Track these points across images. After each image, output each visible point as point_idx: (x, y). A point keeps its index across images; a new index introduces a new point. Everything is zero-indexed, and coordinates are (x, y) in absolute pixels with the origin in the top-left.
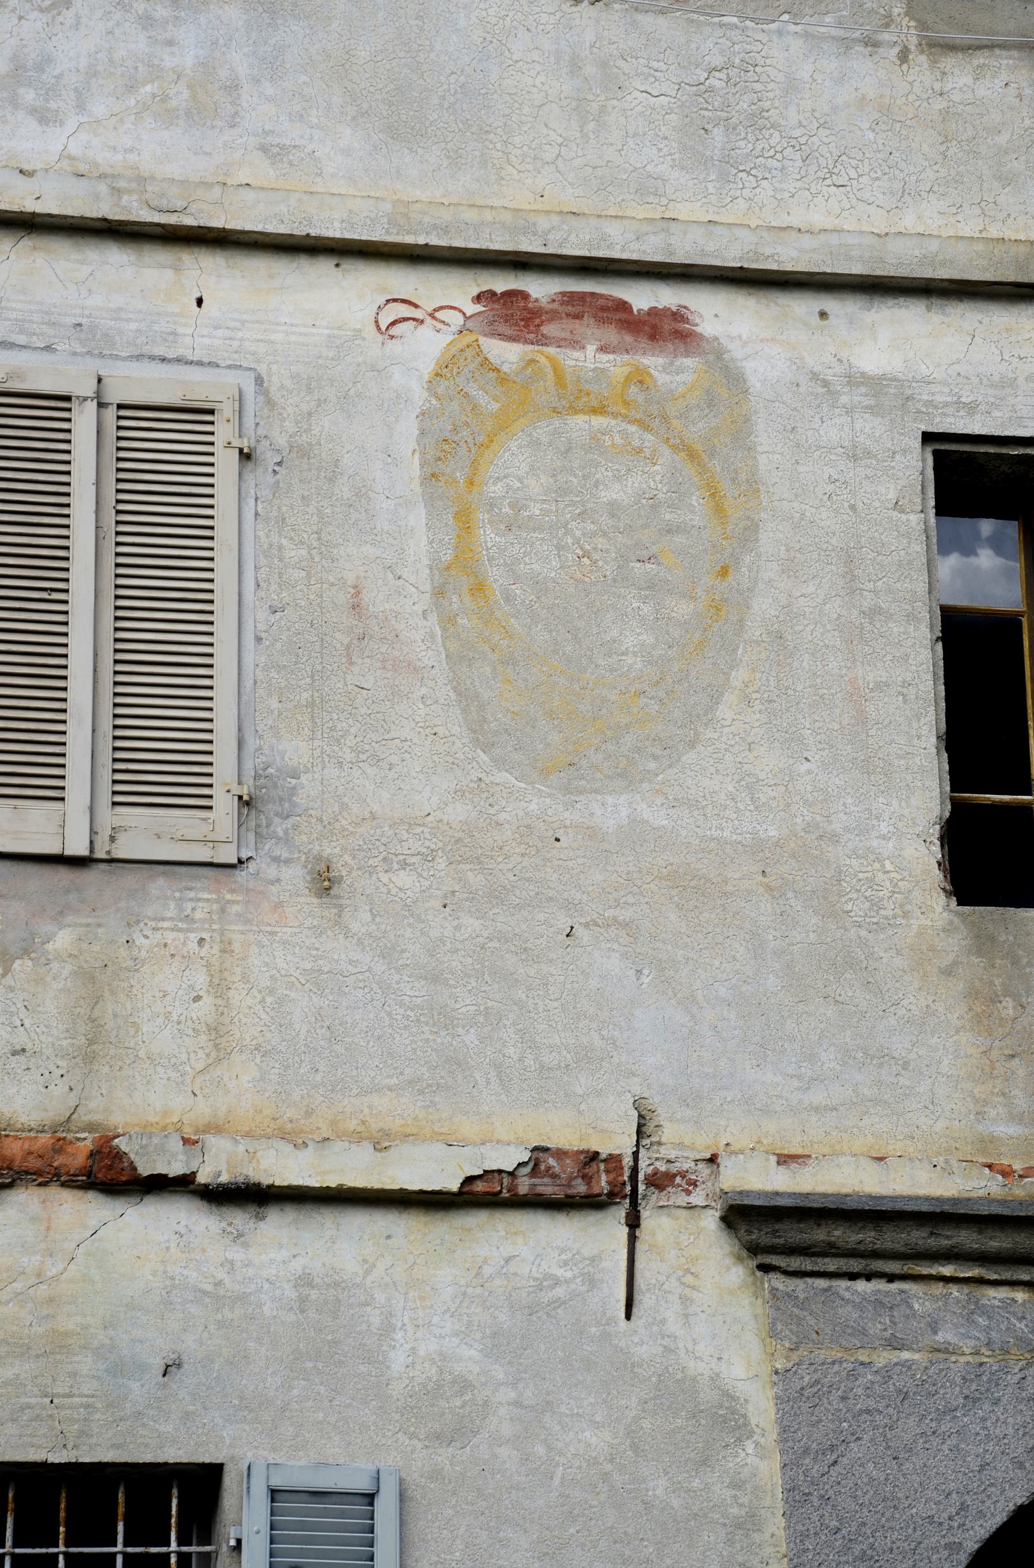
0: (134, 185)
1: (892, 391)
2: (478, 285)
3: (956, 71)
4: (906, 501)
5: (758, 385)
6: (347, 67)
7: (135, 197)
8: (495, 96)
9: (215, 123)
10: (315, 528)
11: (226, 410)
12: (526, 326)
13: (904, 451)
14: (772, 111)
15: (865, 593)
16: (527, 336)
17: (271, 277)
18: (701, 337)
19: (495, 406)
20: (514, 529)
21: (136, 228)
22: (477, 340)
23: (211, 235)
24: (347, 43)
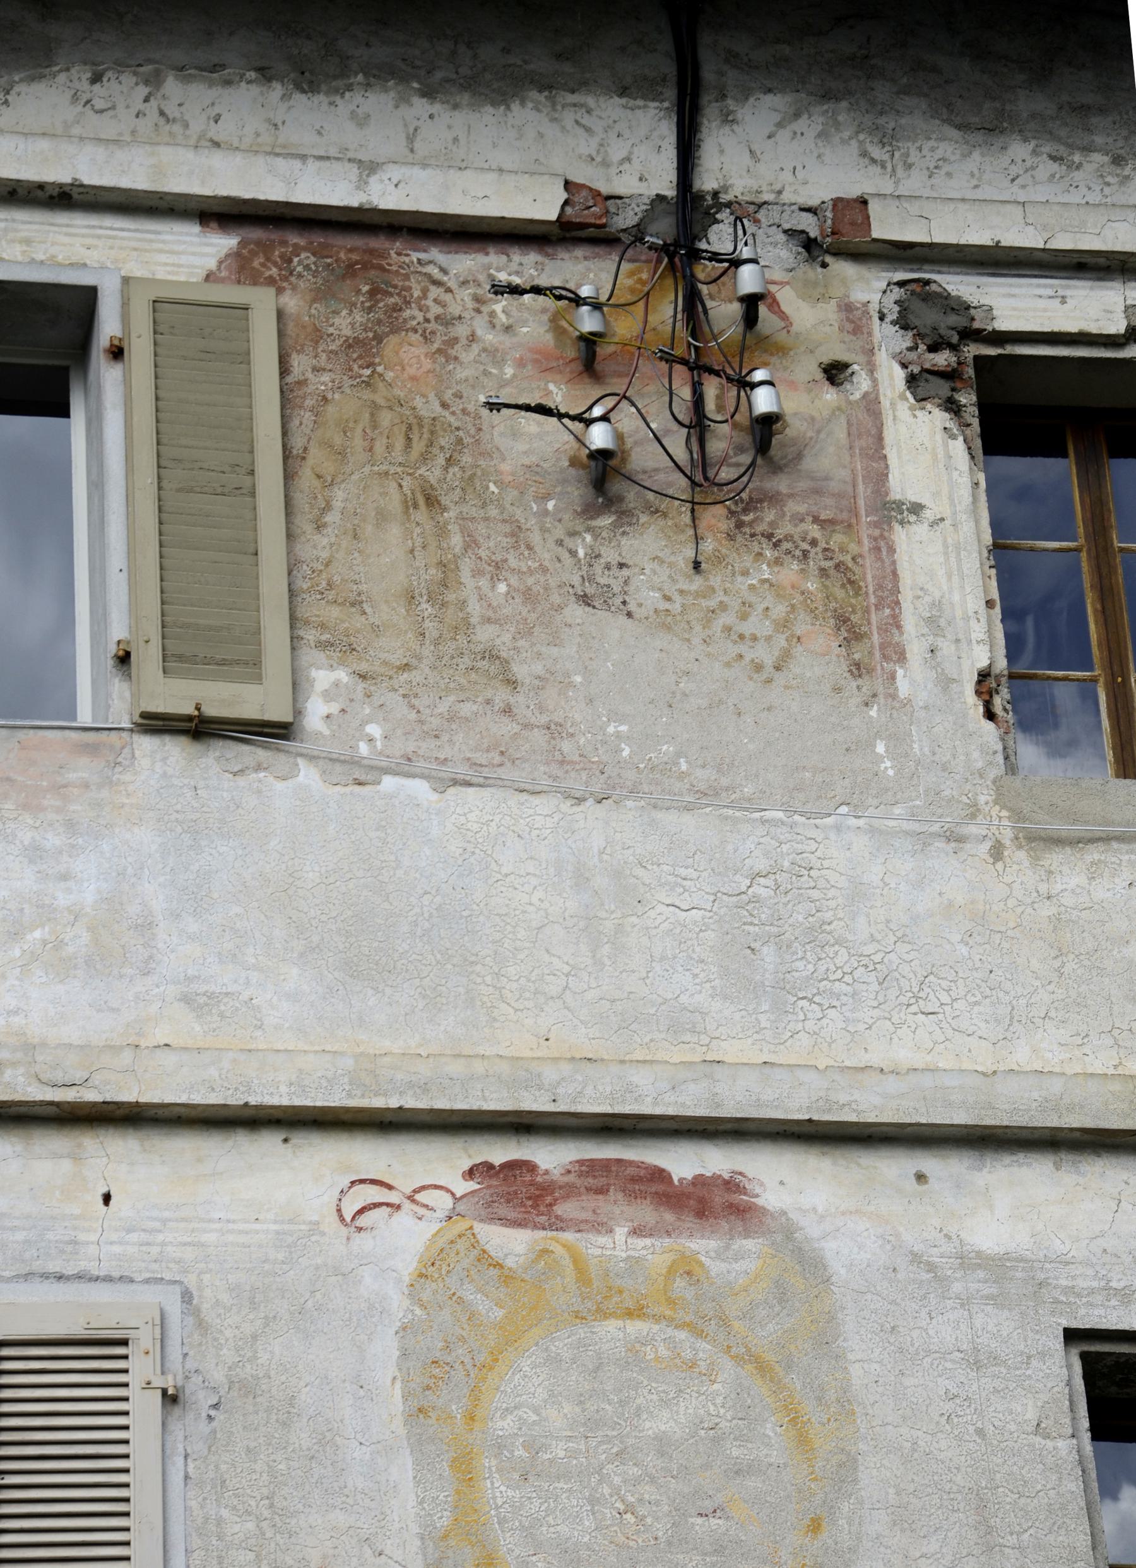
0: (19, 1055)
1: (1019, 1275)
2: (470, 1157)
3: (1065, 869)
4: (1051, 1422)
5: (843, 1271)
6: (290, 892)
7: (21, 1070)
8: (481, 918)
9: (123, 971)
10: (265, 1491)
11: (144, 1339)
12: (535, 1206)
13: (1043, 1355)
14: (835, 923)
15: (1007, 1551)
16: (537, 1219)
17: (199, 1160)
18: (764, 1211)
19: (499, 1313)
20: (531, 1478)
21: (23, 1110)
22: (471, 1228)
23: (120, 1112)
24: (290, 863)
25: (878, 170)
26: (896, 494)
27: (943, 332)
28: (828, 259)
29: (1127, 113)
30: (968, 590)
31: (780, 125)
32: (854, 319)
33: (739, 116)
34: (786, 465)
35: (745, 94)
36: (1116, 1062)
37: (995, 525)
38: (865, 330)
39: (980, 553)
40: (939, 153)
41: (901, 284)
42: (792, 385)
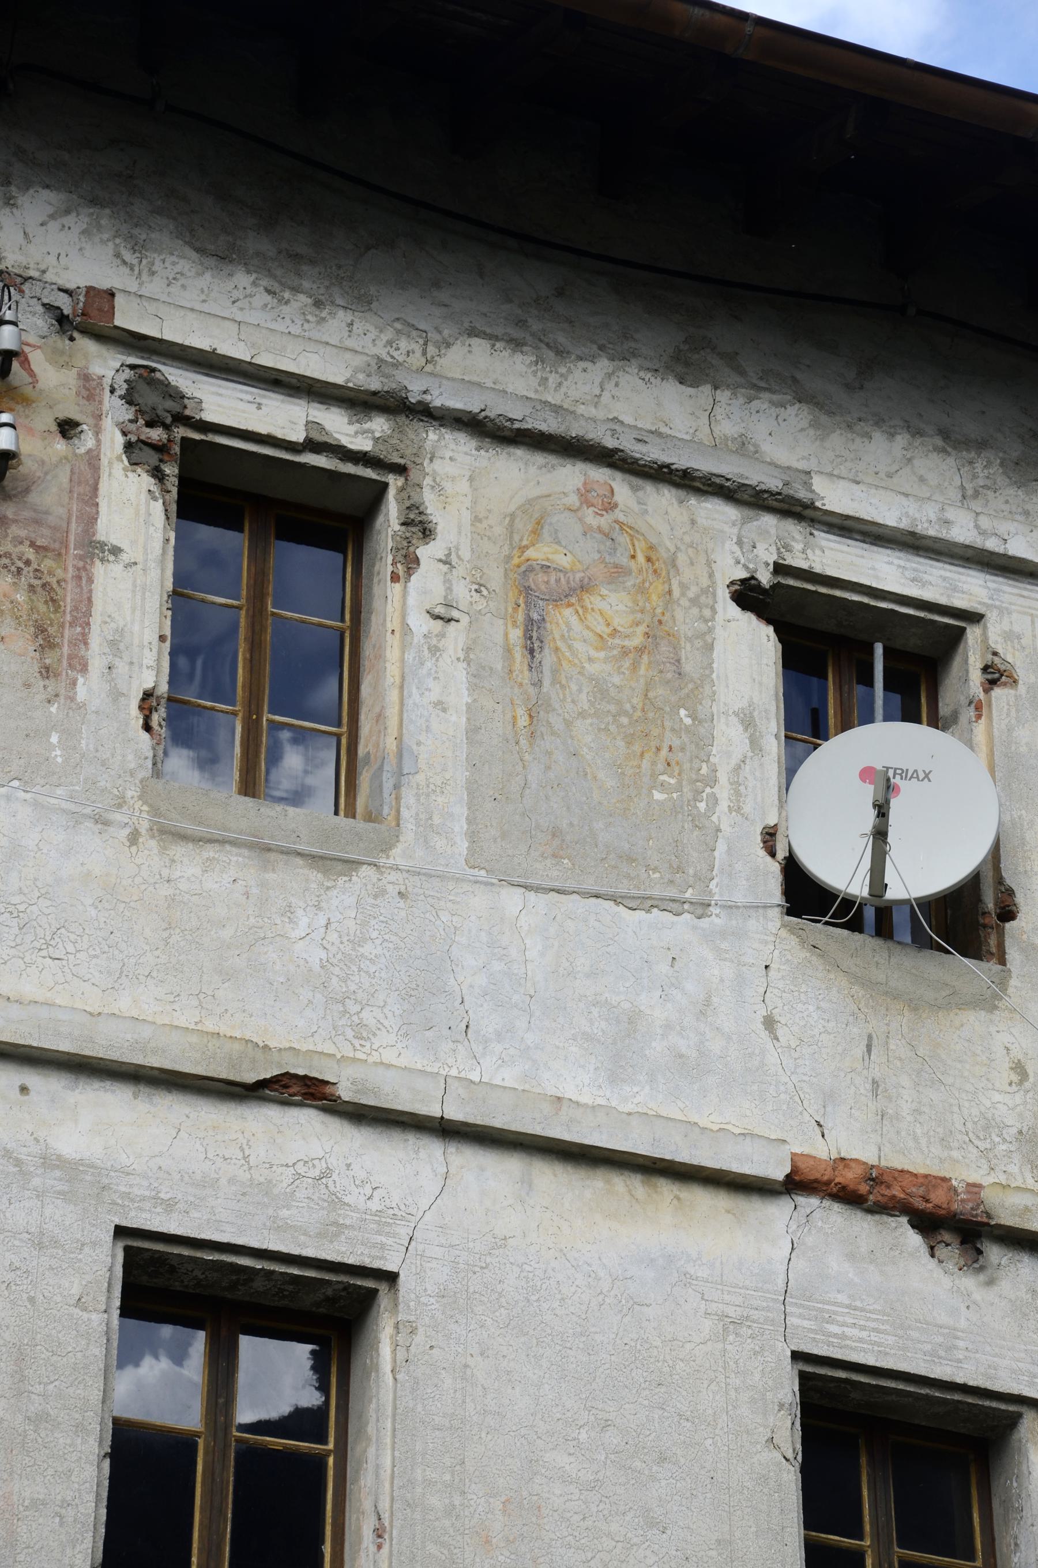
1: (88, 1178)
4: (90, 1298)
13: (94, 1244)
15: (33, 1396)
25: (127, 271)
26: (101, 535)
27: (160, 413)
28: (76, 334)
29: (331, 268)
30: (147, 624)
31: (52, 217)
32: (89, 388)
33: (19, 202)
34: (15, 496)
35: (26, 186)
36: (197, 1019)
37: (179, 578)
38: (97, 398)
39: (161, 597)
40: (178, 268)
41: (132, 367)
42: (30, 431)
